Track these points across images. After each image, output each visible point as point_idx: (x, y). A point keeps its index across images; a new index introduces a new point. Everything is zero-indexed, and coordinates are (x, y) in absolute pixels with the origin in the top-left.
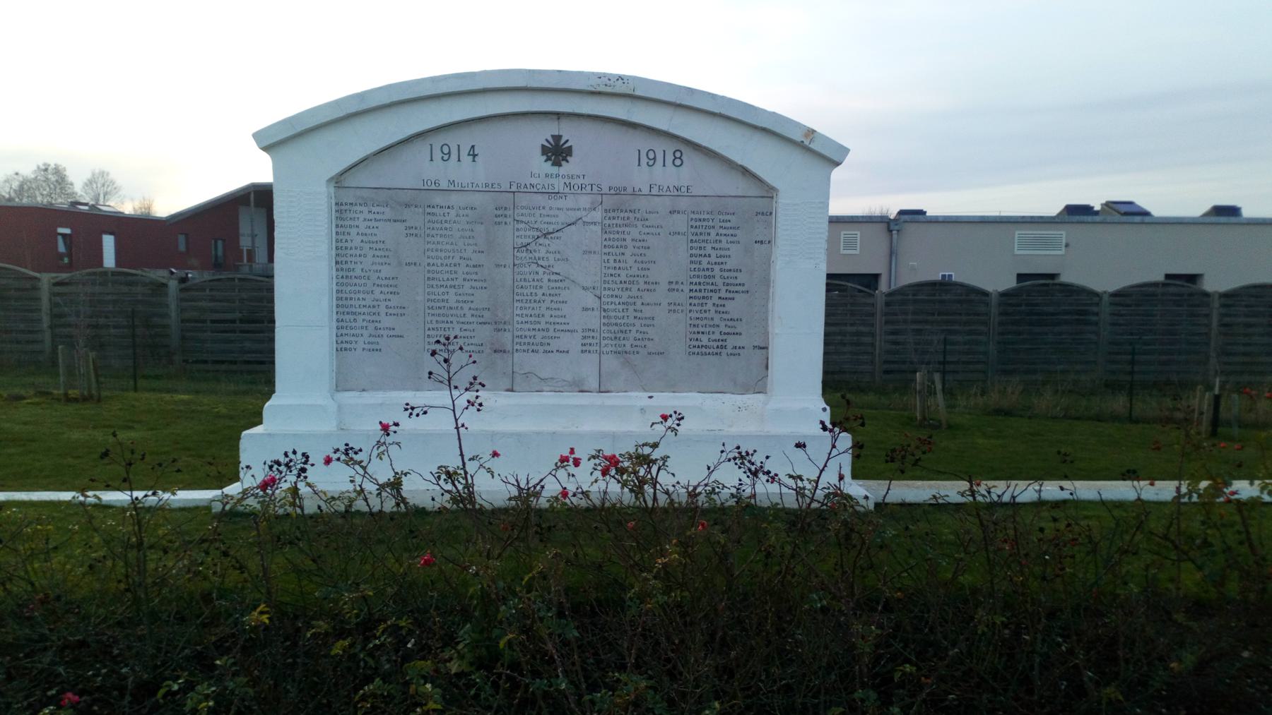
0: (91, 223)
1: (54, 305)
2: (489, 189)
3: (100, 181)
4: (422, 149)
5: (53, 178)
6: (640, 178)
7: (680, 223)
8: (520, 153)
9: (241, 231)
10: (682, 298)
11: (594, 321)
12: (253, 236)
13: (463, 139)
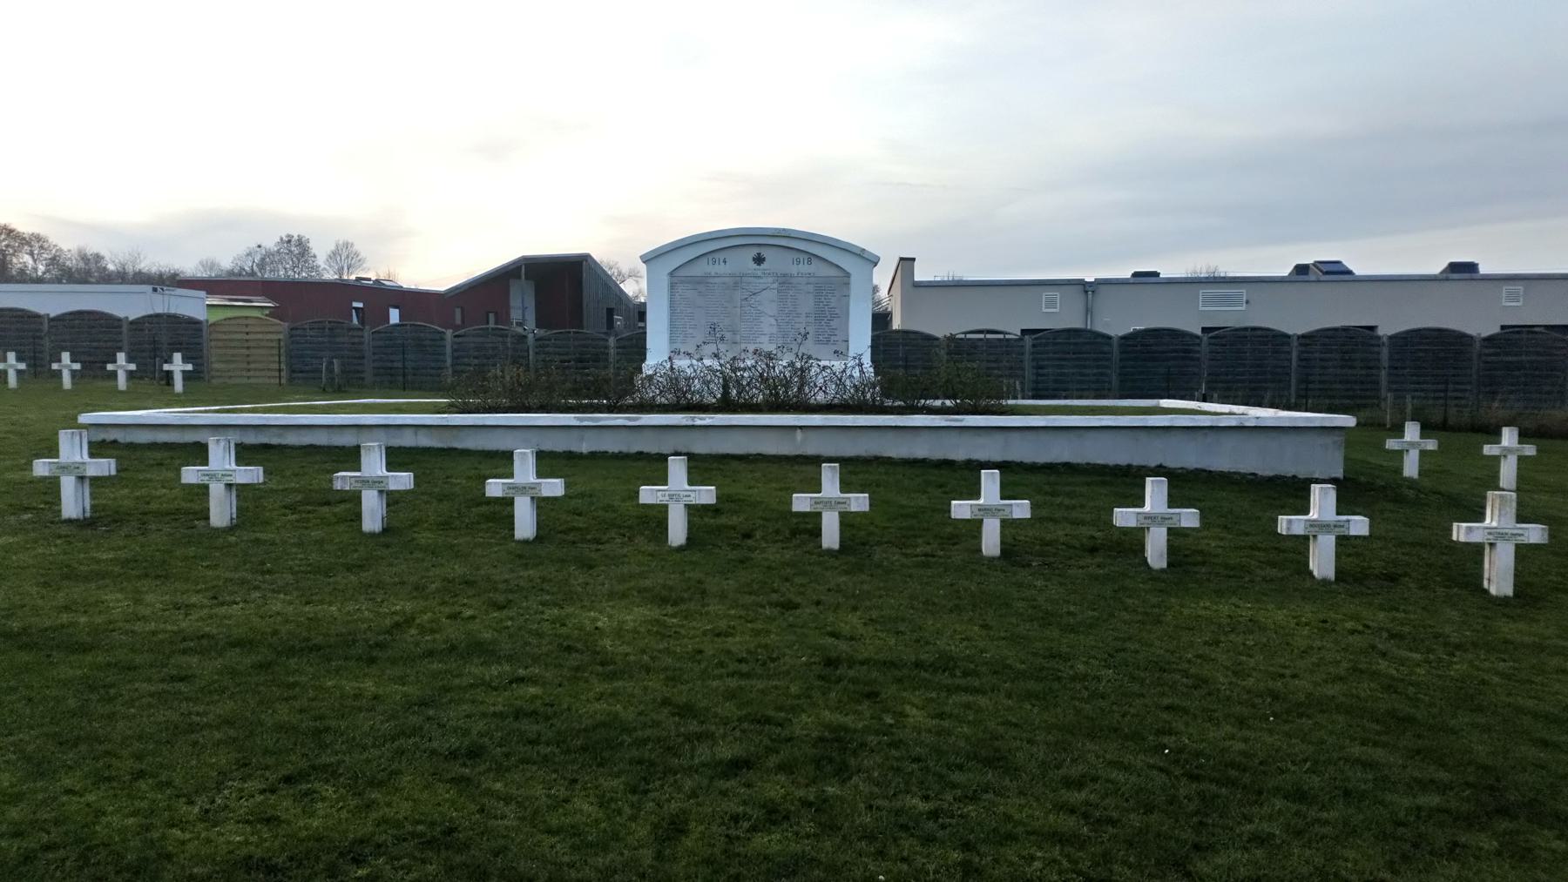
0: (382, 295)
1: (454, 351)
2: (731, 276)
3: (344, 253)
4: (705, 260)
5: (296, 250)
6: (794, 270)
7: (811, 288)
8: (744, 262)
9: (512, 303)
10: (811, 320)
11: (774, 330)
12: (524, 309)
13: (721, 256)
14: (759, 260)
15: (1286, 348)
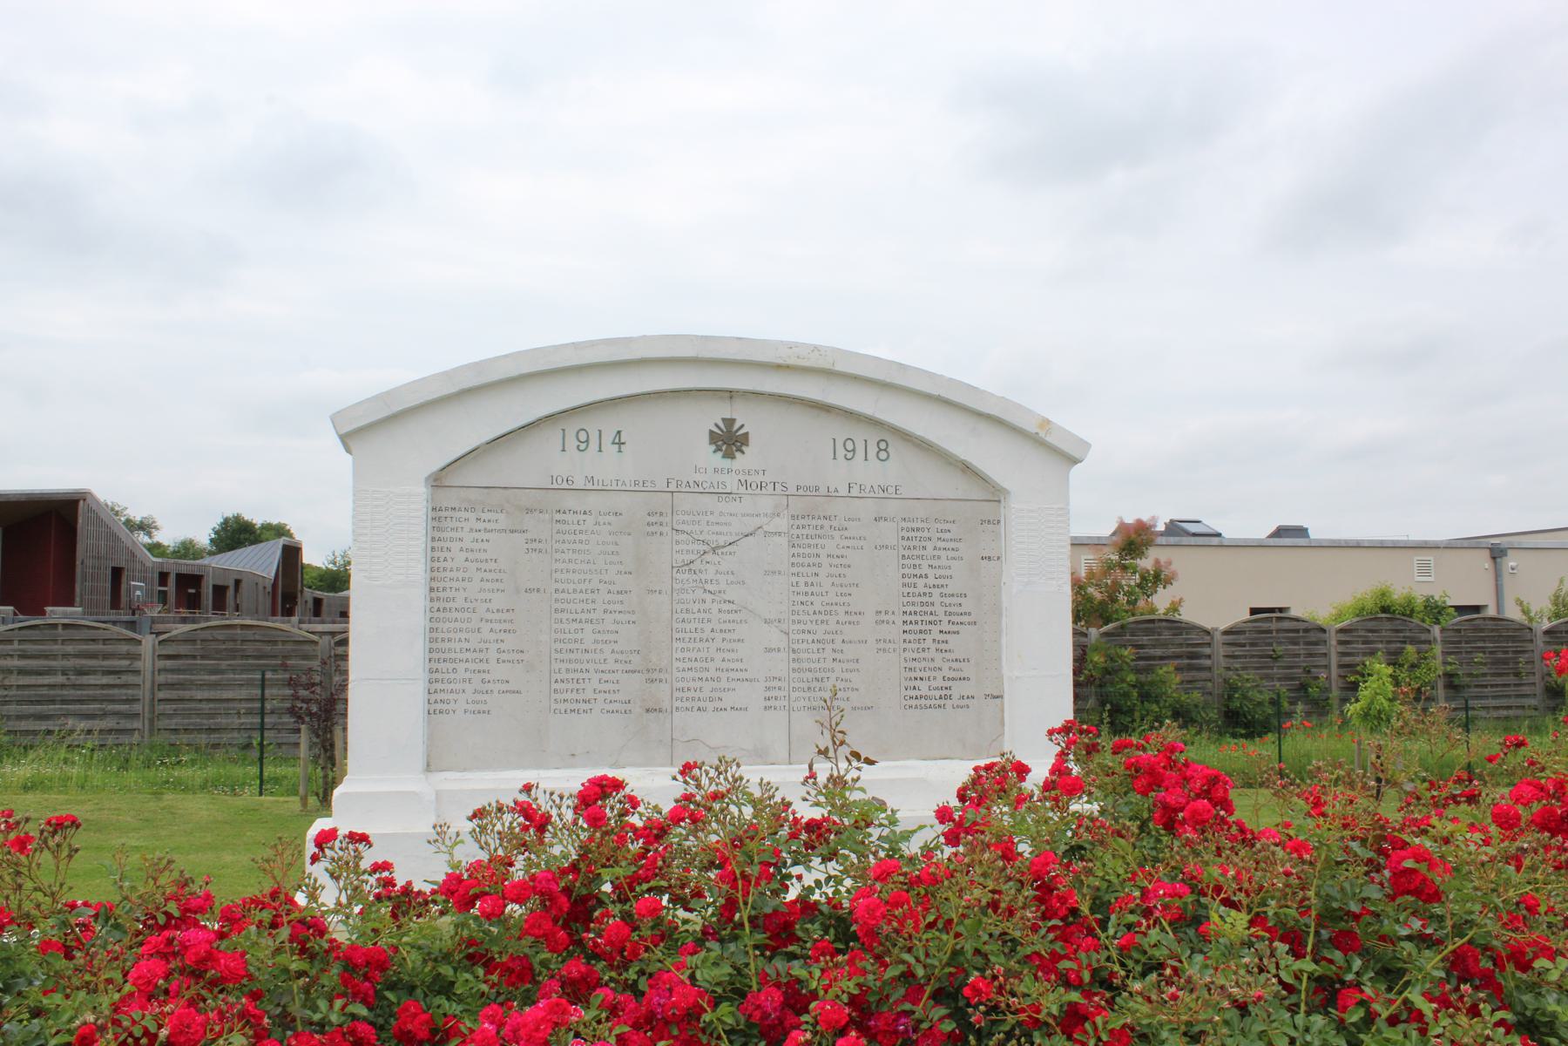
4: (552, 437)
6: (837, 474)
7: (889, 533)
10: (894, 632)
13: (607, 424)
14: (729, 440)
15: (1321, 649)
